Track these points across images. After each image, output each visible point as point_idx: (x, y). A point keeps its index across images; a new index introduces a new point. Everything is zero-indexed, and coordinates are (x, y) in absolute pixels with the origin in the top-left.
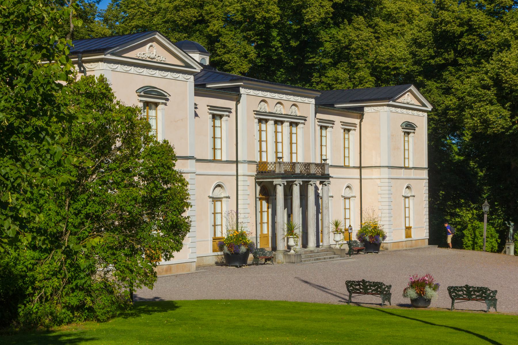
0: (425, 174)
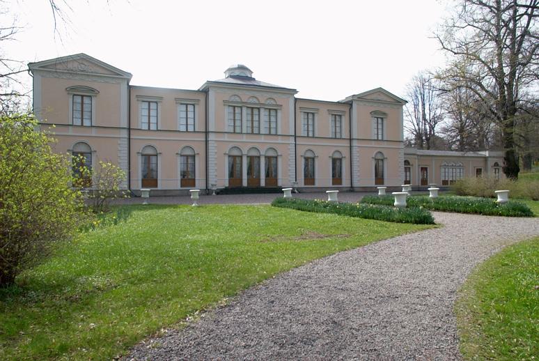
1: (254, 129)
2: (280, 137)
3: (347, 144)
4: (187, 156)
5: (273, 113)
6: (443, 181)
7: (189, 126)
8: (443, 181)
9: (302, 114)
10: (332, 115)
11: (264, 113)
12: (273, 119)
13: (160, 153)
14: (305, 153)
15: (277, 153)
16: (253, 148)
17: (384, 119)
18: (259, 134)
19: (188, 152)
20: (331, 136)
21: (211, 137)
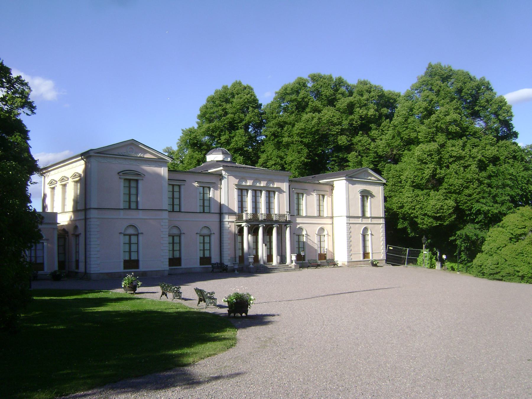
0: (382, 221)
1: (206, 208)
2: (141, 212)
3: (216, 218)
4: (130, 235)
5: (133, 184)
6: (125, 262)
7: (175, 206)
8: (125, 262)
9: (123, 181)
10: (125, 179)
11: (250, 193)
12: (133, 191)
13: (142, 233)
14: (126, 229)
15: (210, 231)
16: (128, 227)
17: (182, 187)
18: (180, 211)
19: (131, 231)
20: (122, 207)
21: (93, 214)
